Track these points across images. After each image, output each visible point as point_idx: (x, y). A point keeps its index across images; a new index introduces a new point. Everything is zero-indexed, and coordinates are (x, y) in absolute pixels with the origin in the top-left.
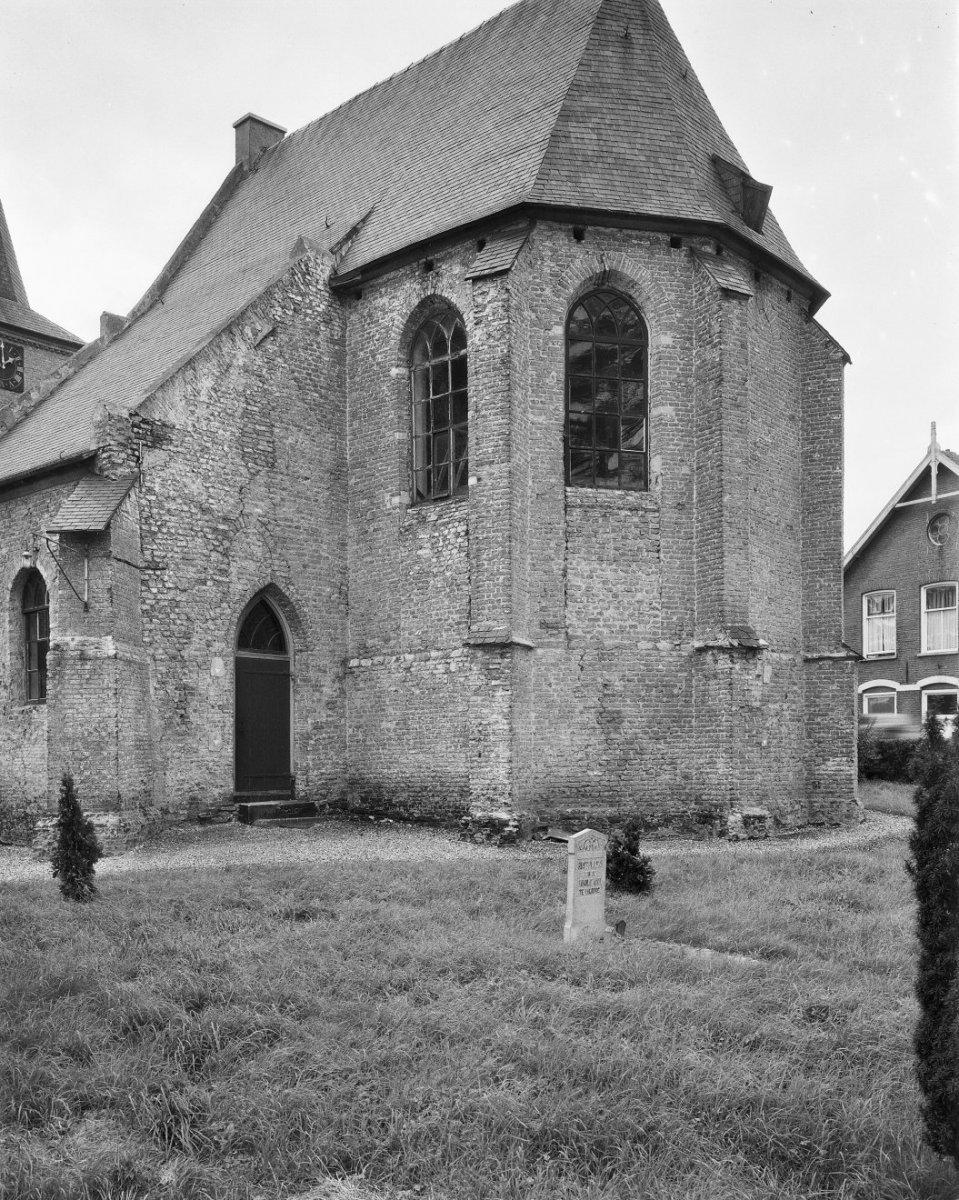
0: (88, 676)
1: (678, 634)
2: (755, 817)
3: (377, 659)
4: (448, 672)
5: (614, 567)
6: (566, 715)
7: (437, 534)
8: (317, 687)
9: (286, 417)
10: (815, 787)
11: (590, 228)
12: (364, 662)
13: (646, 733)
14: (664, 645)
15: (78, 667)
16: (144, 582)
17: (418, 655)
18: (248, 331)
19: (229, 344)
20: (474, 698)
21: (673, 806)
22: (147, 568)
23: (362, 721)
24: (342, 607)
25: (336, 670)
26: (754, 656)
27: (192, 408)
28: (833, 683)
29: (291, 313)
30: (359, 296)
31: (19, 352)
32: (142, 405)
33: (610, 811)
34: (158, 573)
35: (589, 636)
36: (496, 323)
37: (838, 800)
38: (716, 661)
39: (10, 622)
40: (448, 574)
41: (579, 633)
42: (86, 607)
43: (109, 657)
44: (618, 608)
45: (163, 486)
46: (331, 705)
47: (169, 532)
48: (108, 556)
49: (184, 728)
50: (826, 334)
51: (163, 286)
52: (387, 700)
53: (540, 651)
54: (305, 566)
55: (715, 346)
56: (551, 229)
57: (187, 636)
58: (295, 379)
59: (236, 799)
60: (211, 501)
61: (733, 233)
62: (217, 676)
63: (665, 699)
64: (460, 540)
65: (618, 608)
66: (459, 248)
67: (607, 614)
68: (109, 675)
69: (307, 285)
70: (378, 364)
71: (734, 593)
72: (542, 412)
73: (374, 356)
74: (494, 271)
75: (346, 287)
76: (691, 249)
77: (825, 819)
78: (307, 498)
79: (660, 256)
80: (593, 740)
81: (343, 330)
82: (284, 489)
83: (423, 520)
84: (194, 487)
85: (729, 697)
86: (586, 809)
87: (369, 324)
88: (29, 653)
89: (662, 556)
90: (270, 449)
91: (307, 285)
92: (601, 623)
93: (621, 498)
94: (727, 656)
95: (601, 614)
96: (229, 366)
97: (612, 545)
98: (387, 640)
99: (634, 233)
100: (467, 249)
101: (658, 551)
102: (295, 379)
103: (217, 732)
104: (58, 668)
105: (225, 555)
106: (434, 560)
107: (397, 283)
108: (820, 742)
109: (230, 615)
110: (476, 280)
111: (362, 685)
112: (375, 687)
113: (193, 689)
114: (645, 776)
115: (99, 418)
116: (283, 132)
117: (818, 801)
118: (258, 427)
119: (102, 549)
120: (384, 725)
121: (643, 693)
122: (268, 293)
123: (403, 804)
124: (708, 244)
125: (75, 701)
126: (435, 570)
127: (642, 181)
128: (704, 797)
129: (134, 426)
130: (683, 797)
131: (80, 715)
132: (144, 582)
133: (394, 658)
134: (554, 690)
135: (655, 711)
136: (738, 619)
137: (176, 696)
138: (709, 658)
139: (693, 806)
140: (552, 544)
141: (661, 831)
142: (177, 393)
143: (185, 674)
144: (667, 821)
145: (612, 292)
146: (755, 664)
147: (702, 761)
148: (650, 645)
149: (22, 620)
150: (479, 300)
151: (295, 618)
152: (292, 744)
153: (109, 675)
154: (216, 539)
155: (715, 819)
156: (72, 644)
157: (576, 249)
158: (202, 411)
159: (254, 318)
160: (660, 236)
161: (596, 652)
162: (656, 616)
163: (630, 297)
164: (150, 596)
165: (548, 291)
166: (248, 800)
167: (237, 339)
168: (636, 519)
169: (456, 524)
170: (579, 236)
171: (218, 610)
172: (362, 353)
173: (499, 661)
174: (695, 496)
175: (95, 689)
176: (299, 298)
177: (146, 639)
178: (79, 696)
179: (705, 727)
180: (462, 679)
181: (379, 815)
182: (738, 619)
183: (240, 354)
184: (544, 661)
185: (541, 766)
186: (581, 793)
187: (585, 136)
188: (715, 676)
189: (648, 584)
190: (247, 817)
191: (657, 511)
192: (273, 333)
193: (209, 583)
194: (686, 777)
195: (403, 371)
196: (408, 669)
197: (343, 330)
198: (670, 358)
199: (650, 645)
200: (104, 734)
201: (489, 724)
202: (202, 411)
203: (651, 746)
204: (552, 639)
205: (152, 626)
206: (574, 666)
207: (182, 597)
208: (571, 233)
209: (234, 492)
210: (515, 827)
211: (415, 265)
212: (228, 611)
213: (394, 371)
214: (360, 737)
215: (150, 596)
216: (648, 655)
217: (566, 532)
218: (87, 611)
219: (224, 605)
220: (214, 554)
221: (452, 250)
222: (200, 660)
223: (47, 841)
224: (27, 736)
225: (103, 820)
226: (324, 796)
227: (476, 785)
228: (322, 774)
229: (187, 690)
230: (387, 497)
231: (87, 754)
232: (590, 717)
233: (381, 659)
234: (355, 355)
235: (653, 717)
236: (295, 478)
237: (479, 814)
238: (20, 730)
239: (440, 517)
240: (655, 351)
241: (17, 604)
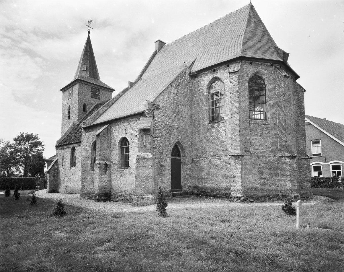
1: (275, 153)
2: (297, 196)
3: (201, 159)
4: (220, 162)
5: (260, 137)
6: (251, 172)
7: (217, 130)
8: (187, 165)
9: (181, 104)
10: (302, 189)
11: (253, 62)
12: (197, 159)
13: (269, 176)
14: (272, 155)
16: (154, 141)
17: (212, 158)
18: (174, 84)
19: (171, 87)
20: (232, 168)
21: (275, 193)
22: (155, 137)
23: (197, 173)
24: (192, 147)
25: (191, 161)
26: (294, 158)
27: (164, 101)
28: (305, 164)
29: (182, 81)
30: (196, 77)
31: (99, 91)
32: (154, 101)
33: (262, 194)
34: (157, 138)
35: (255, 153)
36: (235, 83)
37: (308, 192)
38: (285, 159)
39: (118, 150)
40: (220, 139)
41: (253, 153)
42: (145, 146)
43: (150, 158)
44: (261, 147)
45: (158, 119)
46: (190, 169)
47: (159, 129)
48: (150, 134)
49: (161, 174)
50: (300, 86)
51: (141, 75)
52: (204, 168)
53: (245, 157)
54: (185, 137)
55: (283, 88)
56: (245, 62)
57: (162, 153)
58: (183, 95)
59: (171, 191)
60: (167, 122)
61: (281, 63)
62: (168, 162)
63: (273, 168)
64: (223, 131)
65: (261, 147)
66: (222, 66)
67: (259, 148)
69: (185, 75)
70: (201, 92)
71: (289, 144)
72: (244, 102)
74: (235, 71)
75: (193, 75)
76: (275, 67)
77: (304, 196)
78: (185, 122)
79: (269, 68)
80: (257, 178)
81: (192, 85)
82: (181, 120)
83: (213, 127)
84: (164, 119)
85: (289, 168)
86: (256, 194)
88: (122, 157)
89: (271, 135)
90: (178, 111)
91: (185, 75)
92: (258, 150)
93: (261, 122)
94: (289, 158)
95: (258, 148)
96: (171, 92)
97: (260, 132)
98: (203, 154)
99: (263, 63)
100: (224, 67)
101: (270, 134)
102: (183, 95)
103: (168, 175)
105: (170, 134)
106: (216, 136)
107: (206, 74)
108: (303, 178)
109: (171, 148)
110: (230, 73)
111: (197, 165)
112: (201, 165)
113: (163, 165)
114: (269, 186)
115: (145, 103)
116: (165, 43)
117: (303, 192)
118: (176, 106)
119: (149, 133)
120: (203, 174)
121: (268, 167)
122: (178, 76)
123: (209, 192)
124: (279, 65)
126: (217, 138)
127: (264, 52)
128: (283, 191)
129: (152, 105)
130: (277, 191)
132: (154, 141)
133: (206, 158)
134: (248, 166)
135: (271, 171)
136: (290, 149)
137: (160, 167)
138: (283, 158)
139: (280, 193)
140: (247, 132)
141: (273, 199)
142: (161, 98)
143: (161, 162)
144: (274, 197)
145: (258, 76)
146: (295, 160)
147: (282, 183)
148: (269, 155)
149: (120, 149)
150: (231, 77)
151: (183, 149)
152: (182, 178)
154: (168, 131)
155: (287, 196)
156: (141, 155)
157: (250, 66)
158: (165, 102)
159: (175, 82)
160: (268, 64)
161: (257, 157)
162: (270, 149)
163: (262, 77)
164: (155, 144)
165: (245, 76)
166: (173, 191)
167: (172, 86)
168: (265, 127)
169: (222, 128)
170: (251, 64)
171: (168, 147)
172: (197, 90)
173: (238, 159)
174: (278, 122)
176: (184, 77)
177: (154, 154)
179: (283, 174)
180: (225, 163)
181: (203, 195)
182: (290, 149)
183: (173, 89)
184: (246, 159)
185: (246, 184)
186: (255, 190)
187: (250, 42)
188: (285, 163)
189: (268, 142)
190: (174, 195)
191: (269, 125)
192: (179, 85)
193: (167, 141)
194: (278, 186)
195: (207, 93)
196: (210, 161)
197: (192, 85)
198: (271, 91)
199: (269, 155)
200: (149, 176)
201: (236, 174)
202: (165, 102)
203: (270, 179)
204: (247, 154)
205: (155, 151)
206: (252, 160)
207: (161, 144)
208: (249, 63)
209: (171, 120)
210: (243, 198)
211: (211, 70)
212: (170, 147)
213: (205, 94)
214: (197, 176)
215: (155, 144)
216: (269, 158)
217: (250, 130)
218: (145, 147)
219: (169, 146)
220: (167, 134)
221: (220, 67)
222: (165, 159)
223: (135, 201)
224: (122, 176)
225: (149, 196)
226: (189, 190)
227: (233, 188)
228: (188, 185)
229: (162, 166)
230: (203, 122)
231: (145, 181)
232: (256, 172)
233: (202, 158)
234: (195, 90)
235: (270, 172)
236: (183, 117)
237: (234, 195)
238: (120, 175)
239: (218, 126)
240: (268, 89)
241: (120, 145)
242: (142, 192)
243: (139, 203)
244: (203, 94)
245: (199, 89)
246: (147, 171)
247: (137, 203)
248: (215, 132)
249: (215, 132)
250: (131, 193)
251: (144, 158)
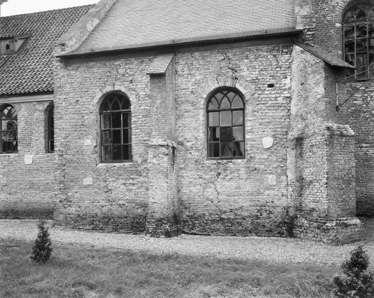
0: (344, 145)
7: (366, 95)
15: (339, 140)
68: (352, 145)
70: (327, 21)
73: (325, 17)
87: (321, 3)
104: (331, 140)
125: (339, 158)
131: (341, 166)
153: (352, 145)
175: (346, 152)
178: (340, 156)
200: (350, 176)
223: (334, 234)
231: (344, 186)
242: (339, 213)
243: (340, 237)
244: (333, 25)
245: (323, 15)
246: (346, 166)
247: (337, 238)
248: (361, 99)
249: (361, 99)
250: (259, 214)
251: (342, 135)
